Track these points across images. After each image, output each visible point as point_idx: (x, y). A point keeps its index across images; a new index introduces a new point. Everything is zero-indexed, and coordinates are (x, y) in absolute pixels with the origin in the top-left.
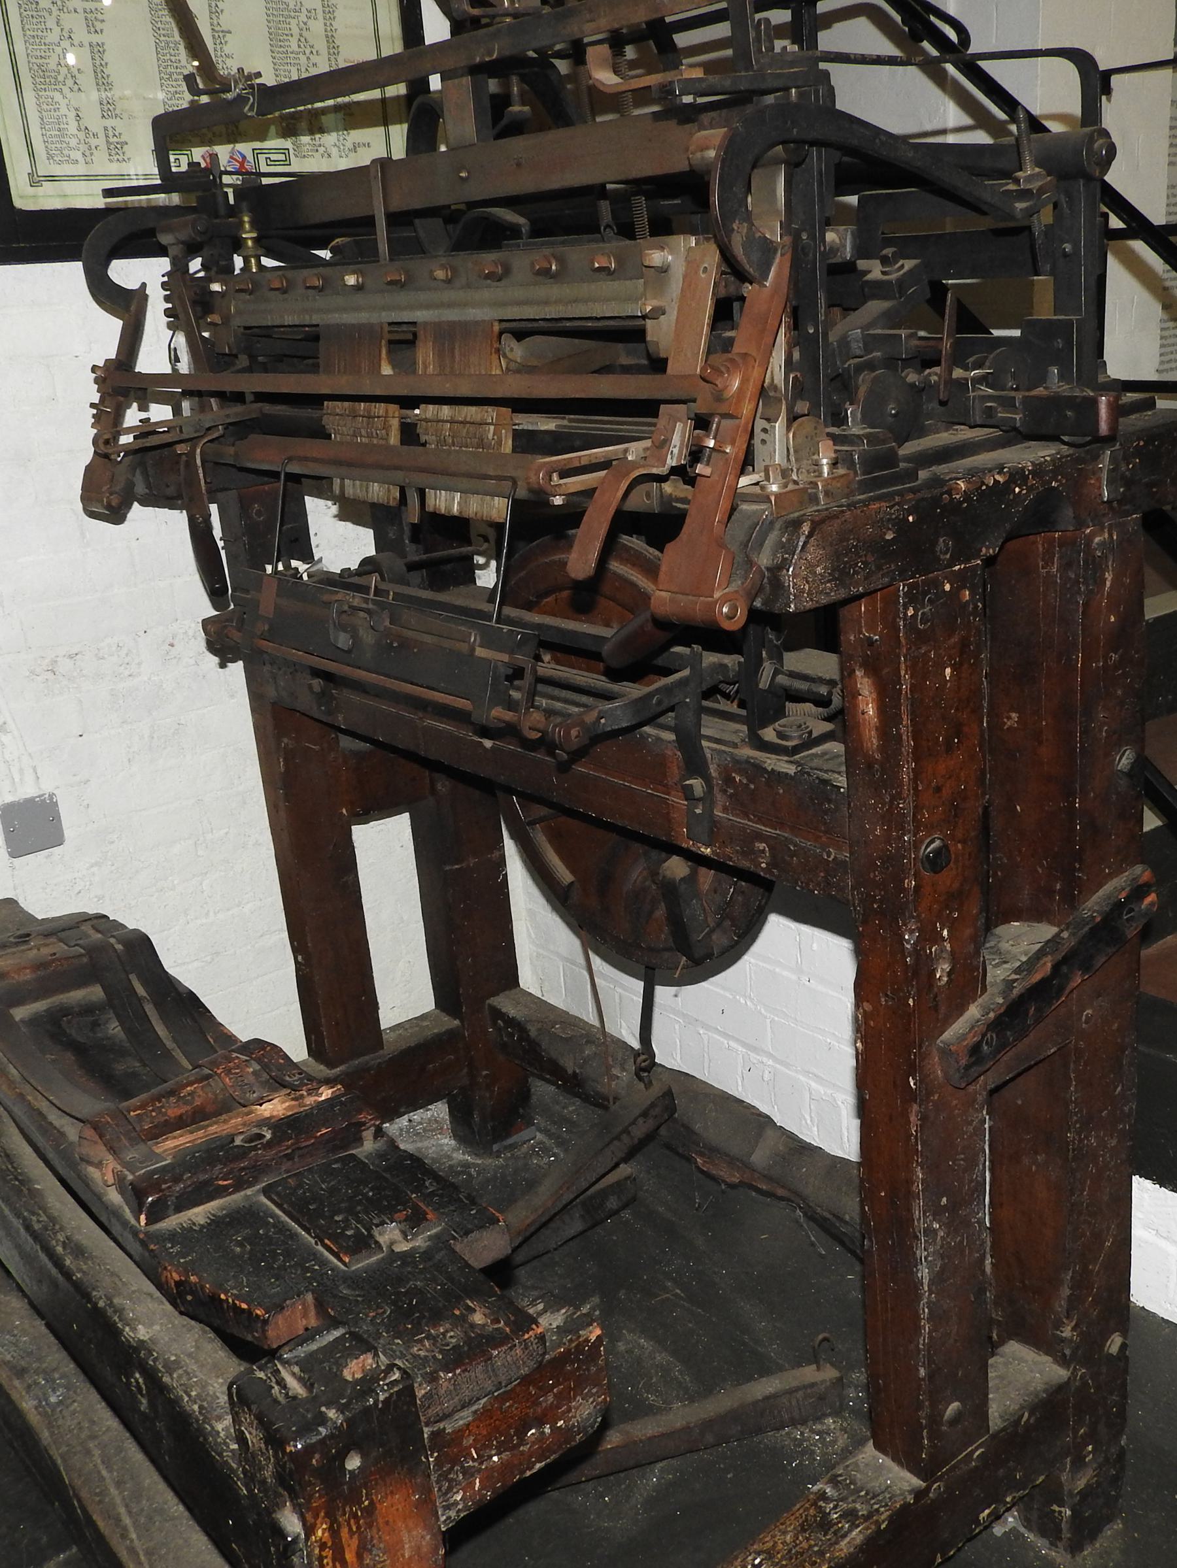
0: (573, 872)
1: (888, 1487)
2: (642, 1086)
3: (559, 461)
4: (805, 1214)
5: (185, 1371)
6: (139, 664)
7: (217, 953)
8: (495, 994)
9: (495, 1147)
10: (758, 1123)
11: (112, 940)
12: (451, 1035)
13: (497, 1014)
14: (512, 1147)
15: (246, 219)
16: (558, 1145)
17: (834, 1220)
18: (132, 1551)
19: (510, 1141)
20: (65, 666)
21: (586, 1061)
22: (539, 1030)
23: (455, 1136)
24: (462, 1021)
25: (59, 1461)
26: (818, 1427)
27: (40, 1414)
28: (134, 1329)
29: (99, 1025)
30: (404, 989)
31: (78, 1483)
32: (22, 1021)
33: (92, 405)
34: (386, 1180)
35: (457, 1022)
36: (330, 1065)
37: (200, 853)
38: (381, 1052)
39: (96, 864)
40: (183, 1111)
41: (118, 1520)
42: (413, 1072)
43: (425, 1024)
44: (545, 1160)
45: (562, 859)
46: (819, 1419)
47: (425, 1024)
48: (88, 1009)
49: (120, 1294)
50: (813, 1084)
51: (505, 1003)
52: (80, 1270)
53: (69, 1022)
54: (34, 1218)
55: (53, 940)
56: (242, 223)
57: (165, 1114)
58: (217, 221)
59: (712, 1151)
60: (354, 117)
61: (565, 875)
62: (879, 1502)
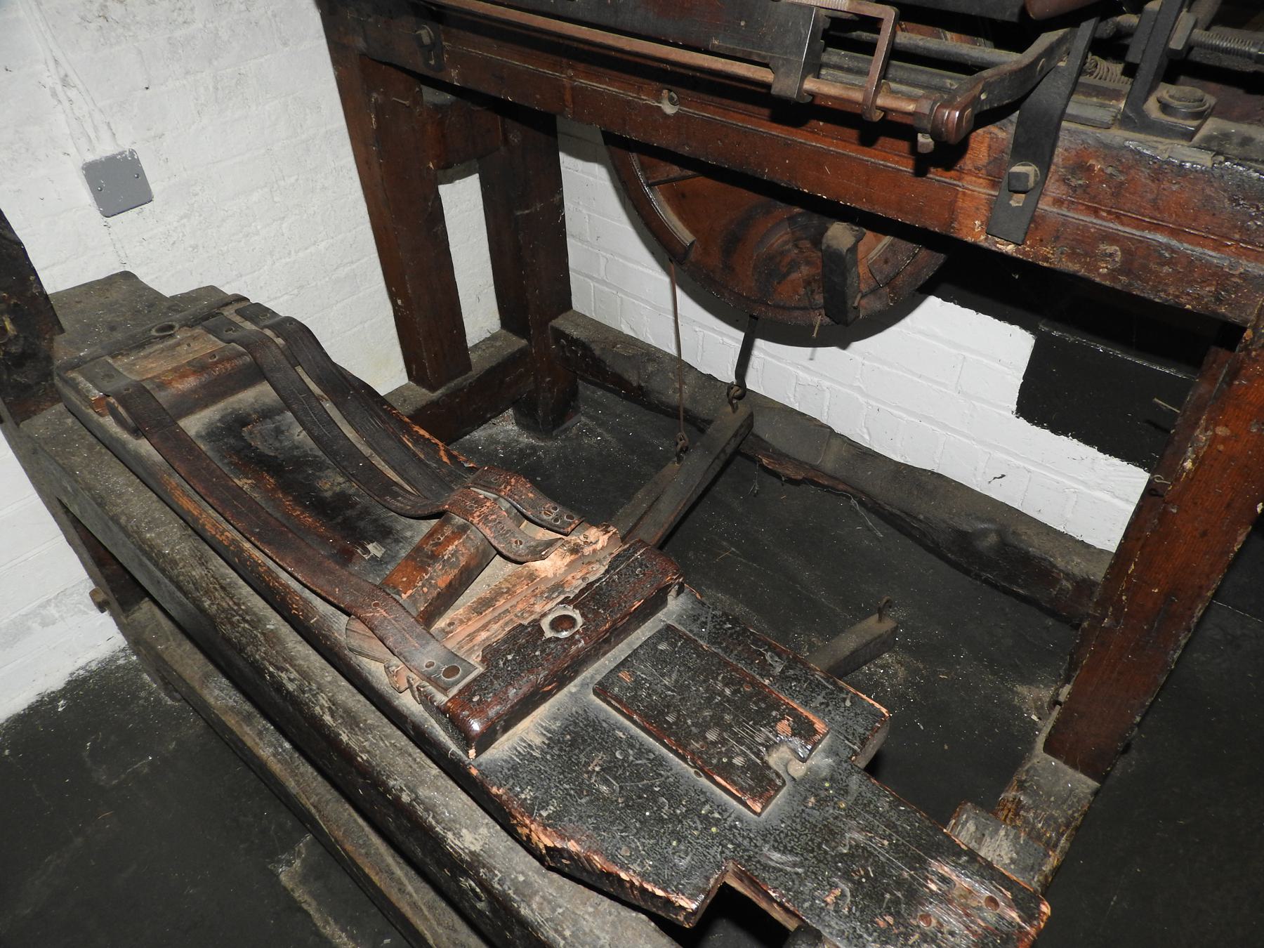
0: (694, 231)
1: (1071, 790)
2: (729, 409)
4: (861, 503)
5: (543, 897)
6: (192, 9)
7: (302, 287)
8: (555, 317)
9: (554, 433)
10: (825, 433)
11: (268, 332)
12: (522, 352)
13: (559, 334)
14: (566, 430)
16: (600, 426)
17: (903, 515)
18: (414, 905)
19: (565, 426)
21: (650, 376)
22: (603, 349)
23: (517, 424)
24: (529, 340)
25: (313, 811)
26: (878, 661)
27: (279, 761)
28: (458, 836)
29: (282, 432)
30: (480, 314)
31: (339, 834)
32: (199, 436)
34: (736, 670)
35: (524, 342)
36: (432, 388)
37: (276, 199)
38: (470, 373)
39: (185, 216)
40: (451, 577)
41: (391, 873)
42: (494, 389)
43: (498, 344)
44: (594, 440)
45: (681, 218)
46: (879, 656)
47: (498, 344)
48: (267, 414)
49: (423, 782)
50: (801, 373)
51: (560, 323)
52: (364, 750)
53: (251, 433)
54: (283, 675)
55: (198, 330)
57: (436, 586)
59: (780, 456)
61: (685, 236)
62: (1070, 807)
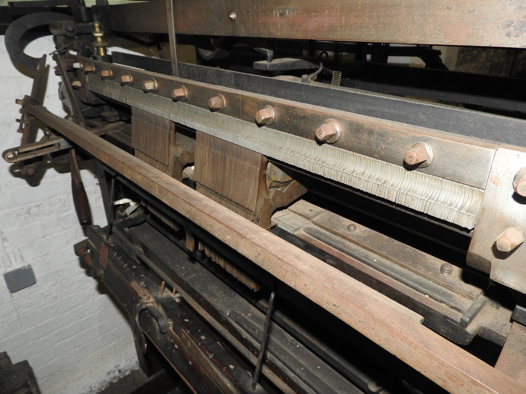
3: (375, 272)
15: (97, 25)
20: (34, 210)
33: (18, 120)
56: (94, 27)
58: (81, 24)
60: (175, 222)
